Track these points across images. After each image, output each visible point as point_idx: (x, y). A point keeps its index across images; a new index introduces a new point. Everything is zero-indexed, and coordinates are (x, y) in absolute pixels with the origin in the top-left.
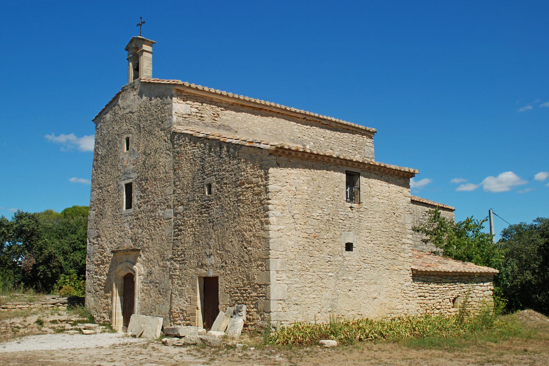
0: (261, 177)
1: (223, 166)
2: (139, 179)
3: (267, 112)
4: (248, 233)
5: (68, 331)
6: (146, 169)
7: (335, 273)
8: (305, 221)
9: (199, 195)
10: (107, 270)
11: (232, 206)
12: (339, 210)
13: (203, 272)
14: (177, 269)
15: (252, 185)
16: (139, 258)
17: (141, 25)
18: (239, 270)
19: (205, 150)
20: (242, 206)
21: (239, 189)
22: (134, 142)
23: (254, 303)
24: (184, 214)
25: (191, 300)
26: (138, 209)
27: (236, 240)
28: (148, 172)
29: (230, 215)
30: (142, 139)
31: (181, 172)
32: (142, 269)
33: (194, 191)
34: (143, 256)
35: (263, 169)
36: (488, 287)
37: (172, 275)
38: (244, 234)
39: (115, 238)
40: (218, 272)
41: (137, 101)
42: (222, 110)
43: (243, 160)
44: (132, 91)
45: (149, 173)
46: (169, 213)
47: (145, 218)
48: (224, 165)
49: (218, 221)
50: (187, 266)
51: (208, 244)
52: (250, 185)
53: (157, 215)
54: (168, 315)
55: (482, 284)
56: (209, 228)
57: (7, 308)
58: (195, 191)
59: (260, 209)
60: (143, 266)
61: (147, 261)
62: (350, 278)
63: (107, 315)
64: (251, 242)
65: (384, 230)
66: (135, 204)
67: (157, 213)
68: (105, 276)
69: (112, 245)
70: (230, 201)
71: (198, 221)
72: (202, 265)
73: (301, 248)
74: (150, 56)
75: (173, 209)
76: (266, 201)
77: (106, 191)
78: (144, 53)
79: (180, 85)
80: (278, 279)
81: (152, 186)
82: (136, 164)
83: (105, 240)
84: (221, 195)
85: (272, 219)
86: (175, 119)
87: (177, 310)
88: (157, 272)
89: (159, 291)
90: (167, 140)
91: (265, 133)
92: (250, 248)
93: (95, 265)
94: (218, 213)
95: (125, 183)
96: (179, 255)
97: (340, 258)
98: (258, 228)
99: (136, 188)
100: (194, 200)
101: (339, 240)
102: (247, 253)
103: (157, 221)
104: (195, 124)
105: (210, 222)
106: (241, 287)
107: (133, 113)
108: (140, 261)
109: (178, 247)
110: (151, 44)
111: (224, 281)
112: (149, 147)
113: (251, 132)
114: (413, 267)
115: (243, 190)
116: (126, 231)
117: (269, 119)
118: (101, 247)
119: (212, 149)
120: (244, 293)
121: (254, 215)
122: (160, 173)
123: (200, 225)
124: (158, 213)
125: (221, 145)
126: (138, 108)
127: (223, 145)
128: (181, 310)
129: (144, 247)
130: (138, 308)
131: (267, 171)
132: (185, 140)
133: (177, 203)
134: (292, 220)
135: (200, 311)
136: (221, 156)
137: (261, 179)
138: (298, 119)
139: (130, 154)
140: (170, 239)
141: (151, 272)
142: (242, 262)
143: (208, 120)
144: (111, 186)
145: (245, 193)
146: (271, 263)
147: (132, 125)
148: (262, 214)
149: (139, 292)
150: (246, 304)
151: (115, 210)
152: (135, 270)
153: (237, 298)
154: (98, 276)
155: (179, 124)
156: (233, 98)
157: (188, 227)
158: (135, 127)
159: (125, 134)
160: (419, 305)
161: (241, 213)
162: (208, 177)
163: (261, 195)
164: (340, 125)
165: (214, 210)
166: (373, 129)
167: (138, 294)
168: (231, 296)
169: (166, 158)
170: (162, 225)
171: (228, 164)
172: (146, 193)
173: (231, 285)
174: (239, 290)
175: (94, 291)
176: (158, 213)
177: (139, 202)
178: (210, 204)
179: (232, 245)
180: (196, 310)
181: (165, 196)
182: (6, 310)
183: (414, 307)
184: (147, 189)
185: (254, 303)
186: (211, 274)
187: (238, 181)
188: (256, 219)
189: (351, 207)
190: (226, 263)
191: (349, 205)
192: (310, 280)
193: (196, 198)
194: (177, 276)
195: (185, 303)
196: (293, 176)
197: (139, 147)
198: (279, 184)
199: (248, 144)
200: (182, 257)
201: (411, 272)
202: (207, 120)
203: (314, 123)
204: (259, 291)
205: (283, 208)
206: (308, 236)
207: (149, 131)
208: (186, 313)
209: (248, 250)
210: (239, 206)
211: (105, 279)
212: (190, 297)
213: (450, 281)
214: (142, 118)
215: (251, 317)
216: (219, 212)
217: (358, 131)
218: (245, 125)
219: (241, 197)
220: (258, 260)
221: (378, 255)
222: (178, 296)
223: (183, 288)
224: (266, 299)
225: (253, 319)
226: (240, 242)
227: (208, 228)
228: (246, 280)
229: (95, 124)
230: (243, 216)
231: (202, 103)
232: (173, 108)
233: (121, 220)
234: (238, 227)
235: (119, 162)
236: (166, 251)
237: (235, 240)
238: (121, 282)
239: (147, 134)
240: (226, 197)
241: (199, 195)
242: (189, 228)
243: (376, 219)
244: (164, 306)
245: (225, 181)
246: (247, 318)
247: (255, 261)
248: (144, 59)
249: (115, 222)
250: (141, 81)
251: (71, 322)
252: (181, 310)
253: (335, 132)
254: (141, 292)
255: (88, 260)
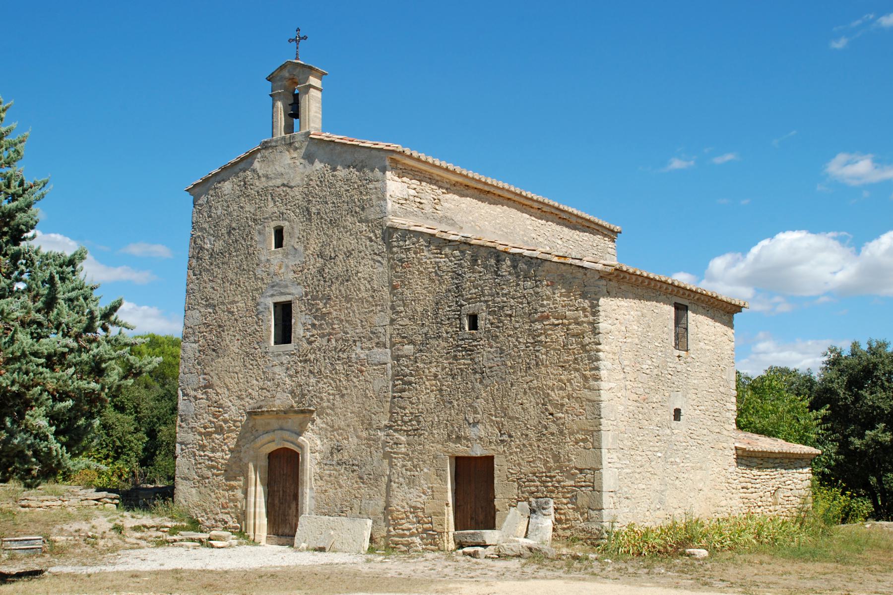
0: (584, 310)
1: (503, 289)
2: (309, 297)
3: (496, 198)
4: (557, 392)
5: (182, 543)
6: (325, 281)
7: (664, 452)
8: (635, 376)
9: (450, 330)
10: (232, 444)
11: (523, 351)
12: (668, 360)
13: (462, 450)
14: (401, 444)
15: (566, 321)
16: (309, 425)
17: (297, 42)
18: (539, 446)
19: (462, 261)
20: (544, 350)
21: (538, 326)
22: (296, 236)
23: (569, 495)
24: (416, 358)
25: (433, 491)
26: (305, 345)
27: (531, 402)
28: (330, 286)
29: (518, 363)
30: (313, 231)
31: (407, 292)
32: (319, 442)
33: (438, 323)
34: (318, 421)
35: (587, 299)
36: (802, 478)
37: (391, 452)
38: (548, 394)
39: (250, 391)
40: (494, 450)
41: (300, 169)
42: (443, 193)
43: (545, 283)
44: (289, 151)
45: (333, 288)
46: (384, 355)
47: (325, 359)
48: (504, 287)
49: (492, 372)
50: (425, 439)
51: (471, 406)
52: (560, 321)
53: (353, 356)
54: (381, 516)
55: (801, 470)
56: (474, 381)
57: (29, 506)
58: (441, 324)
59: (581, 357)
60: (320, 438)
61: (330, 429)
62: (678, 460)
63: (232, 518)
64: (562, 405)
65: (710, 390)
66: (300, 337)
67: (354, 354)
68: (227, 452)
69: (243, 403)
70: (519, 342)
71: (447, 369)
72: (459, 438)
73: (631, 416)
74: (318, 94)
75: (391, 348)
76: (594, 346)
77: (224, 312)
78: (311, 89)
79: (400, 152)
80: (610, 460)
81: (340, 310)
82: (301, 271)
83: (226, 392)
84: (500, 332)
85: (603, 373)
86: (390, 206)
87: (403, 507)
88: (353, 447)
89: (361, 478)
90: (373, 238)
91: (493, 230)
92: (560, 415)
93: (200, 434)
94: (493, 360)
95: (275, 301)
96: (406, 423)
97: (668, 431)
98: (577, 386)
99: (301, 312)
100: (439, 337)
101: (668, 404)
102: (554, 422)
103: (353, 366)
104: (414, 215)
105: (476, 372)
106: (543, 472)
107: (291, 187)
108: (312, 430)
109: (404, 409)
110: (321, 75)
111: (505, 463)
112: (332, 246)
113: (478, 229)
114: (737, 445)
115: (547, 327)
116: (278, 379)
117: (498, 209)
118: (215, 405)
119: (479, 261)
120: (548, 482)
121: (570, 366)
122: (359, 290)
123: (453, 376)
124: (356, 354)
125: (498, 256)
126: (303, 180)
127: (503, 257)
128: (411, 507)
129: (322, 407)
130: (310, 505)
131: (595, 302)
132: (418, 242)
133: (400, 340)
134: (622, 375)
135: (451, 509)
136: (499, 272)
137: (583, 312)
138: (532, 210)
139: (286, 255)
140: (385, 397)
141: (339, 448)
142: (544, 435)
143: (428, 209)
144: (239, 304)
145: (550, 332)
146: (603, 438)
147: (289, 207)
148: (586, 365)
149: (313, 480)
150: (552, 498)
151: (250, 344)
152: (303, 443)
153: (533, 489)
154: (206, 453)
155: (395, 214)
156: (461, 175)
157: (425, 379)
158: (298, 211)
159: (272, 221)
160: (741, 500)
161: (542, 362)
162: (469, 304)
163: (584, 337)
164: (580, 221)
165: (483, 356)
166: (618, 227)
167: (311, 482)
168: (519, 485)
169: (372, 266)
170: (365, 374)
171: (513, 286)
172: (325, 320)
173: (521, 469)
174: (537, 477)
175: (196, 477)
176: (356, 354)
177: (308, 334)
178: (476, 346)
179: (523, 409)
180: (446, 507)
181: (370, 327)
182: (27, 509)
183: (737, 504)
184: (330, 313)
185: (569, 495)
186: (478, 451)
187: (536, 313)
188: (573, 372)
189: (679, 356)
190: (510, 436)
191: (677, 353)
192: (640, 463)
193: (445, 335)
194: (401, 454)
195: (420, 497)
196: (623, 311)
197: (308, 244)
198: (610, 322)
199: (556, 259)
200: (412, 425)
201: (734, 452)
202: (427, 209)
203: (550, 217)
204: (580, 478)
205: (613, 357)
206: (638, 399)
207: (331, 220)
208: (424, 512)
209: (556, 418)
210: (538, 351)
211: (228, 457)
212: (432, 487)
213: (772, 465)
214: (313, 197)
215: (563, 517)
216: (495, 359)
217: (600, 229)
218: (471, 218)
219: (543, 338)
220: (578, 432)
221: (704, 427)
222: (404, 485)
223: (416, 473)
224: (594, 490)
225: (567, 520)
226: (540, 405)
227: (471, 382)
228: (552, 461)
229: (192, 197)
230: (547, 366)
231: (420, 181)
232: (388, 188)
233: (265, 362)
234: (535, 382)
235: (258, 265)
236: (375, 415)
237: (530, 402)
238: (264, 463)
239: (325, 224)
240: (510, 336)
241: (450, 330)
242: (428, 380)
243: (702, 374)
244: (372, 502)
245: (509, 312)
246: (555, 519)
247: (571, 434)
248: (311, 101)
249: (252, 365)
250: (311, 136)
251: (166, 529)
252: (411, 507)
253: (573, 231)
254: (315, 480)
255: (180, 426)
